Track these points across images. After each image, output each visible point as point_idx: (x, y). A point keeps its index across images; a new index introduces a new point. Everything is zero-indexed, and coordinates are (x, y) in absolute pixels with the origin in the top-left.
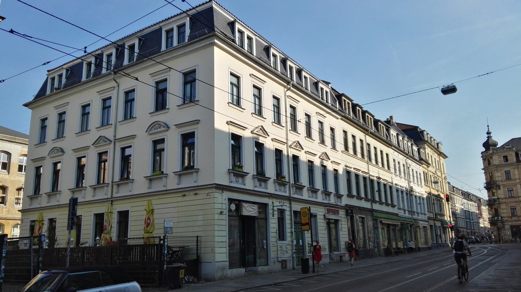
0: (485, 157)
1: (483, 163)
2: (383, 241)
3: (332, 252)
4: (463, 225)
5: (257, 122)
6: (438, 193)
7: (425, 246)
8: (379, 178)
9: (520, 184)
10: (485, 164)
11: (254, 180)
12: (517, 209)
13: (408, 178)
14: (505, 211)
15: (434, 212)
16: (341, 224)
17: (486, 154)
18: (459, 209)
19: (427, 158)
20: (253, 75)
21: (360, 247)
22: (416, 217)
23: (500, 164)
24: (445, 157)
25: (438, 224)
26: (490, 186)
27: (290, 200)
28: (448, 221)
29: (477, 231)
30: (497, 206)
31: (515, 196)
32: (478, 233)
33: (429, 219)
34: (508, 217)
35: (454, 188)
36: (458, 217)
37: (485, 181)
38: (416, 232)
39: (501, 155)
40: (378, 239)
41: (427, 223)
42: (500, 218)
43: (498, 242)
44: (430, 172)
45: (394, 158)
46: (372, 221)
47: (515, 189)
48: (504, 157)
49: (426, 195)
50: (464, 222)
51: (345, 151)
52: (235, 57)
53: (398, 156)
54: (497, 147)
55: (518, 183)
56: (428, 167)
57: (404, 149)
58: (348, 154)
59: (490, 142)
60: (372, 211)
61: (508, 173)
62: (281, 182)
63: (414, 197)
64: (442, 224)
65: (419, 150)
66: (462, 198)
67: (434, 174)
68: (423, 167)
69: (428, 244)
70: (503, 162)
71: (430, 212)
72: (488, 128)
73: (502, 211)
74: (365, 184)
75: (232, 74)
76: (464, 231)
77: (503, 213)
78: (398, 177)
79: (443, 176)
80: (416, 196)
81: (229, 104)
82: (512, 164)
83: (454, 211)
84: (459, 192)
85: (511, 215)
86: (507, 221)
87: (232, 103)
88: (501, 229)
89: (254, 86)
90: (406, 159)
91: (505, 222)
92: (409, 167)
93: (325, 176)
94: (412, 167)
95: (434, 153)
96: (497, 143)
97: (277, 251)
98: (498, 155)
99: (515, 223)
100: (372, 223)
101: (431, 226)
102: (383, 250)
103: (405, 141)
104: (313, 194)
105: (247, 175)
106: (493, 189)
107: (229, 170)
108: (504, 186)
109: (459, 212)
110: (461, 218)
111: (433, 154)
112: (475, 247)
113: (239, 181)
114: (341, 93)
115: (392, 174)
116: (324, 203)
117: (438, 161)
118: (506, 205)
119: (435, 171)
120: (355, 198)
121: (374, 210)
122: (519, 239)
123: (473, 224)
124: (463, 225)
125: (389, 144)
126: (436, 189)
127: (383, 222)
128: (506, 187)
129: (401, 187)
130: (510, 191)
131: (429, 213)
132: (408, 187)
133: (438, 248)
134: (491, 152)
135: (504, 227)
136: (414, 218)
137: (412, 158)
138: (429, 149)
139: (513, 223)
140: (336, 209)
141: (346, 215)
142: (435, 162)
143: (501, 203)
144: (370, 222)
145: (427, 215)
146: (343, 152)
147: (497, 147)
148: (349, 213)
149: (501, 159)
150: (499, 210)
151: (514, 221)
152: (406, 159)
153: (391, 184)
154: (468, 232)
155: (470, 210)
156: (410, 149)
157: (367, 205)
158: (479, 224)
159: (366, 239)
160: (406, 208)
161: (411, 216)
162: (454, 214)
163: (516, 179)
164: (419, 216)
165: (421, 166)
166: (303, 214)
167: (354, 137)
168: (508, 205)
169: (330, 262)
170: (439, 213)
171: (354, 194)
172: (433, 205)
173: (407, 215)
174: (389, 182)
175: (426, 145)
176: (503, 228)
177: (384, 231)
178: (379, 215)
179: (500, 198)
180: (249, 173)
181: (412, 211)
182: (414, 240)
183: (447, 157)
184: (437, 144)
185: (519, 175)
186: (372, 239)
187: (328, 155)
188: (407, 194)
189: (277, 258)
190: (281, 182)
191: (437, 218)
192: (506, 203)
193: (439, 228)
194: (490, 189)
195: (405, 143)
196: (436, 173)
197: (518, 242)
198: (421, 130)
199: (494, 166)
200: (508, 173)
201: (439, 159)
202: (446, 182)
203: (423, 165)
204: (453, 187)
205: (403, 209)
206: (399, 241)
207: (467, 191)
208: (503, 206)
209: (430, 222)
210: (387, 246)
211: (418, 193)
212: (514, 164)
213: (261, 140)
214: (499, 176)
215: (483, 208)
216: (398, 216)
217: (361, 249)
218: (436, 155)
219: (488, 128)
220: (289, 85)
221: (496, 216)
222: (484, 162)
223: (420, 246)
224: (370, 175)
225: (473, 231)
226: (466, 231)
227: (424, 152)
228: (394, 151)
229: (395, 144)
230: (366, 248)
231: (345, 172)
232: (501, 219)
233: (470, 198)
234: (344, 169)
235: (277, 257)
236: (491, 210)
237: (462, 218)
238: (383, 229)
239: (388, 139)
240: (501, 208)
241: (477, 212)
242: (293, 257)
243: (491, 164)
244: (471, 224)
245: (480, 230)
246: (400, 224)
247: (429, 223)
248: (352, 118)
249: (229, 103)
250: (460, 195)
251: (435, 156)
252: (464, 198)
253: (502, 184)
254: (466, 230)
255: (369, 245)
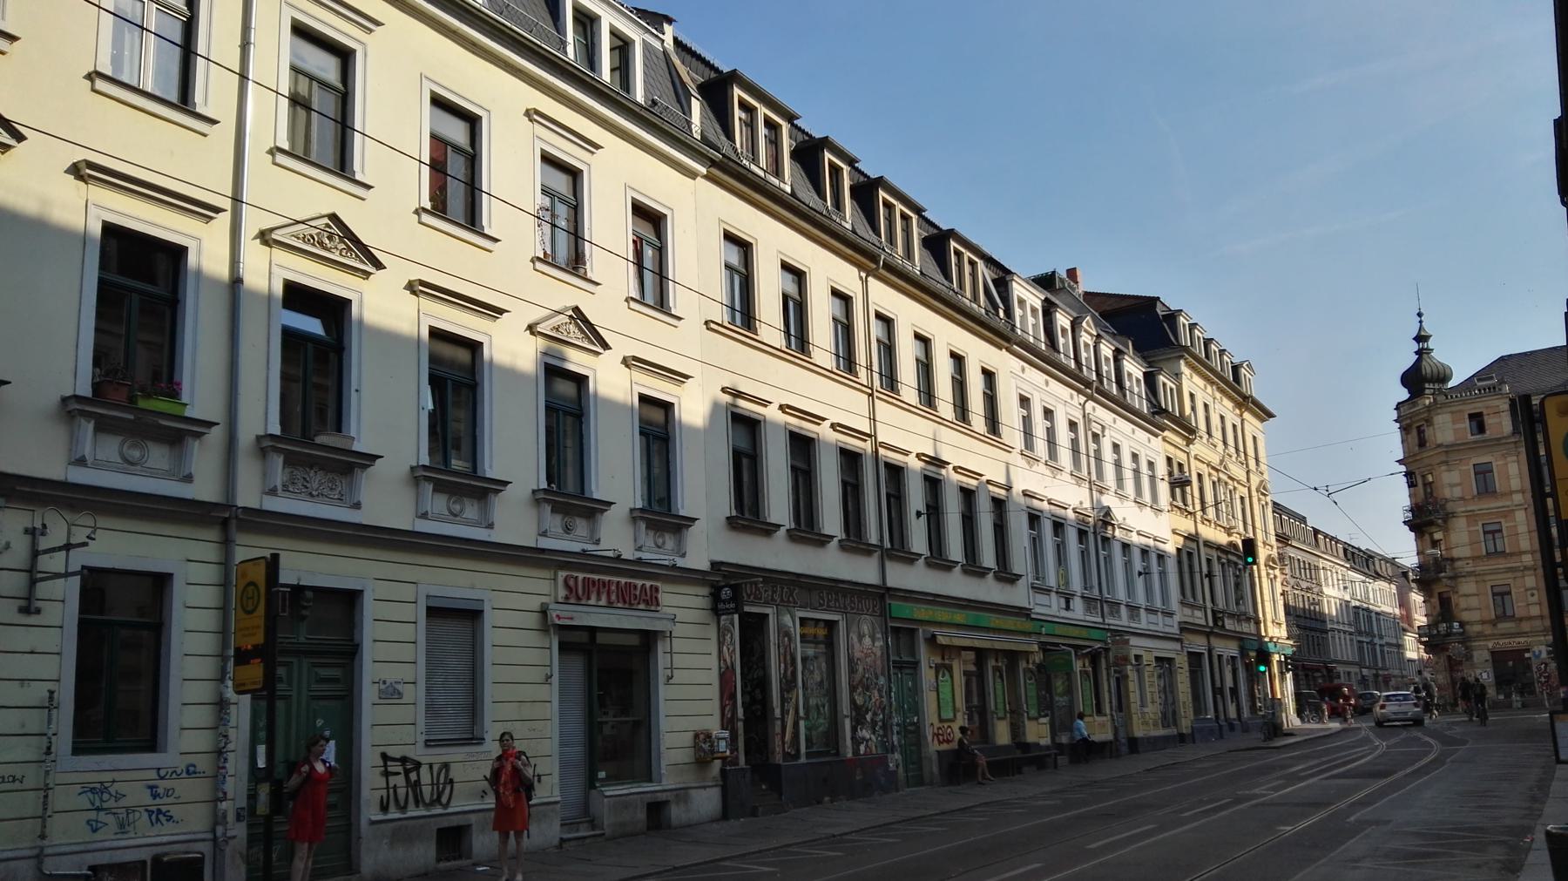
0: (1408, 421)
1: (1402, 442)
2: (941, 720)
3: (595, 788)
4: (1348, 655)
5: (561, 293)
6: (1232, 539)
7: (1161, 732)
8: (938, 462)
9: (1526, 509)
10: (1408, 444)
11: (635, 524)
12: (1513, 593)
13: (1089, 473)
14: (1474, 602)
15: (1209, 604)
16: (671, 652)
17: (1412, 411)
18: (1336, 604)
19: (1188, 411)
20: (537, 112)
21: (798, 751)
22: (1123, 620)
23: (1458, 442)
24: (1264, 414)
25: (1229, 649)
26: (1422, 520)
27: (225, 524)
28: (1267, 639)
29: (1396, 672)
30: (1447, 586)
31: (1507, 551)
32: (1400, 679)
33: (1182, 630)
34: (1483, 622)
35: (1319, 536)
36: (1329, 626)
37: (1407, 502)
38: (1121, 680)
39: (1460, 411)
40: (917, 714)
41: (1177, 646)
42: (1456, 625)
43: (1448, 708)
44: (1197, 462)
45: (1150, 459)
46: (879, 636)
47: (1507, 527)
48: (1471, 416)
49: (1176, 543)
50: (1352, 645)
51: (987, 434)
52: (645, 148)
53: (1045, 387)
54: (1451, 384)
55: (1516, 506)
56: (1189, 442)
57: (1099, 374)
58: (1001, 446)
59: (1426, 368)
60: (882, 594)
61: (1483, 472)
62: (132, 417)
63: (1117, 550)
64: (1243, 651)
65: (1150, 380)
66: (1347, 568)
67: (1213, 468)
68: (1164, 439)
69: (1175, 724)
70: (1469, 435)
71: (1192, 607)
72: (1421, 322)
73: (1463, 603)
74: (999, 523)
75: (438, 102)
76: (1349, 673)
77: (1466, 609)
78: (1149, 509)
79: (1255, 480)
80: (1126, 547)
81: (92, 81)
82: (1498, 442)
83: (1307, 607)
84: (1334, 547)
85: (1493, 617)
86: (1480, 636)
87: (638, 298)
88: (1460, 663)
89: (548, 159)
90: (1085, 402)
91: (1475, 641)
92: (1099, 432)
93: (581, 423)
94: (1113, 434)
95: (1218, 395)
96: (1448, 371)
97: (43, 818)
98: (1452, 412)
99: (1507, 641)
100: (879, 644)
101: (1195, 658)
102: (935, 757)
103: (1083, 333)
104: (663, 536)
105: (502, 488)
106: (1433, 529)
107: (534, 492)
108: (1471, 517)
109: (1334, 613)
110: (1339, 631)
111: (1214, 398)
112: (460, 869)
113: (664, 543)
114: (944, 227)
115: (1010, 452)
116: (543, 551)
117: (1234, 426)
118: (1477, 582)
119: (1222, 462)
120: (991, 575)
121: (889, 589)
122: (1518, 698)
123: (1382, 652)
124: (1348, 655)
125: (1002, 335)
126: (1220, 523)
127: (941, 640)
128: (1476, 521)
129: (1053, 507)
130: (1493, 533)
131: (1185, 609)
132: (1087, 504)
133: (1221, 737)
134: (1427, 402)
135: (1469, 657)
136: (1112, 627)
137: (1120, 405)
138: (1197, 379)
139: (1501, 642)
140: (596, 577)
141: (712, 609)
142: (1220, 429)
143: (1463, 576)
144: (867, 641)
145: (1177, 618)
146: (713, 326)
147: (1451, 384)
148: (724, 602)
149: (1462, 426)
150: (1454, 599)
151: (1504, 635)
152: (1085, 402)
153: (1003, 492)
154: (1363, 677)
155: (1371, 607)
156: (1108, 369)
157: (863, 571)
158: (1401, 651)
159: (839, 715)
160: (1076, 584)
161: (1100, 620)
162: (1318, 617)
163: (1511, 493)
164: (1139, 620)
165: (1156, 436)
166: (245, 598)
167: (923, 340)
168: (1484, 581)
169: (562, 840)
170: (1233, 608)
171: (985, 565)
172: (1206, 581)
173: (1078, 611)
174: (988, 482)
175: (1182, 362)
176: (1467, 660)
177: (952, 677)
178: (921, 612)
179: (1459, 559)
180: (697, 519)
181: (1103, 601)
182: (1108, 711)
183: (1270, 415)
184: (1236, 369)
185: (1521, 478)
186: (875, 714)
187: (365, 246)
188: (1082, 534)
189: (39, 857)
190: (131, 417)
191: (1223, 626)
192: (1479, 575)
193: (1228, 664)
194: (1424, 529)
195: (1087, 345)
196: (1226, 469)
197: (1515, 705)
198: (1170, 310)
199: (1440, 450)
200: (1483, 472)
201: (1239, 421)
202: (1267, 503)
203: (1166, 433)
204: (1316, 532)
205: (1057, 593)
206: (1029, 718)
207: (1367, 549)
208: (1467, 587)
209: (1188, 640)
210: (961, 741)
211: (1139, 533)
212: (1504, 441)
213: (577, 361)
214: (1453, 482)
215: (1417, 600)
216: (1028, 616)
217: (803, 760)
218: (1229, 404)
219: (1421, 322)
220: (1090, 389)
221: (1444, 621)
222: (1405, 436)
223: (1139, 732)
224: (878, 445)
225: (1381, 672)
226: (1356, 674)
227: (1174, 386)
228: (1150, 436)
229: (1031, 340)
230: (837, 754)
231: (724, 422)
232: (1461, 630)
233: (1371, 567)
234: (716, 406)
235: (35, 852)
236: (1429, 601)
237: (1345, 632)
238: (942, 669)
239: (998, 315)
240: (1461, 593)
241: (1397, 611)
242: (215, 839)
243: (1428, 445)
244: (1375, 649)
245: (1405, 670)
246: (1036, 648)
247: (1182, 647)
248: (918, 273)
249: (93, 75)
250: (1337, 557)
251: (1224, 407)
252: (1352, 568)
253: (1464, 509)
254: (1358, 670)
255: (852, 738)
